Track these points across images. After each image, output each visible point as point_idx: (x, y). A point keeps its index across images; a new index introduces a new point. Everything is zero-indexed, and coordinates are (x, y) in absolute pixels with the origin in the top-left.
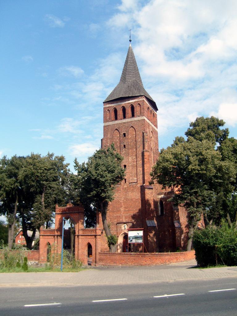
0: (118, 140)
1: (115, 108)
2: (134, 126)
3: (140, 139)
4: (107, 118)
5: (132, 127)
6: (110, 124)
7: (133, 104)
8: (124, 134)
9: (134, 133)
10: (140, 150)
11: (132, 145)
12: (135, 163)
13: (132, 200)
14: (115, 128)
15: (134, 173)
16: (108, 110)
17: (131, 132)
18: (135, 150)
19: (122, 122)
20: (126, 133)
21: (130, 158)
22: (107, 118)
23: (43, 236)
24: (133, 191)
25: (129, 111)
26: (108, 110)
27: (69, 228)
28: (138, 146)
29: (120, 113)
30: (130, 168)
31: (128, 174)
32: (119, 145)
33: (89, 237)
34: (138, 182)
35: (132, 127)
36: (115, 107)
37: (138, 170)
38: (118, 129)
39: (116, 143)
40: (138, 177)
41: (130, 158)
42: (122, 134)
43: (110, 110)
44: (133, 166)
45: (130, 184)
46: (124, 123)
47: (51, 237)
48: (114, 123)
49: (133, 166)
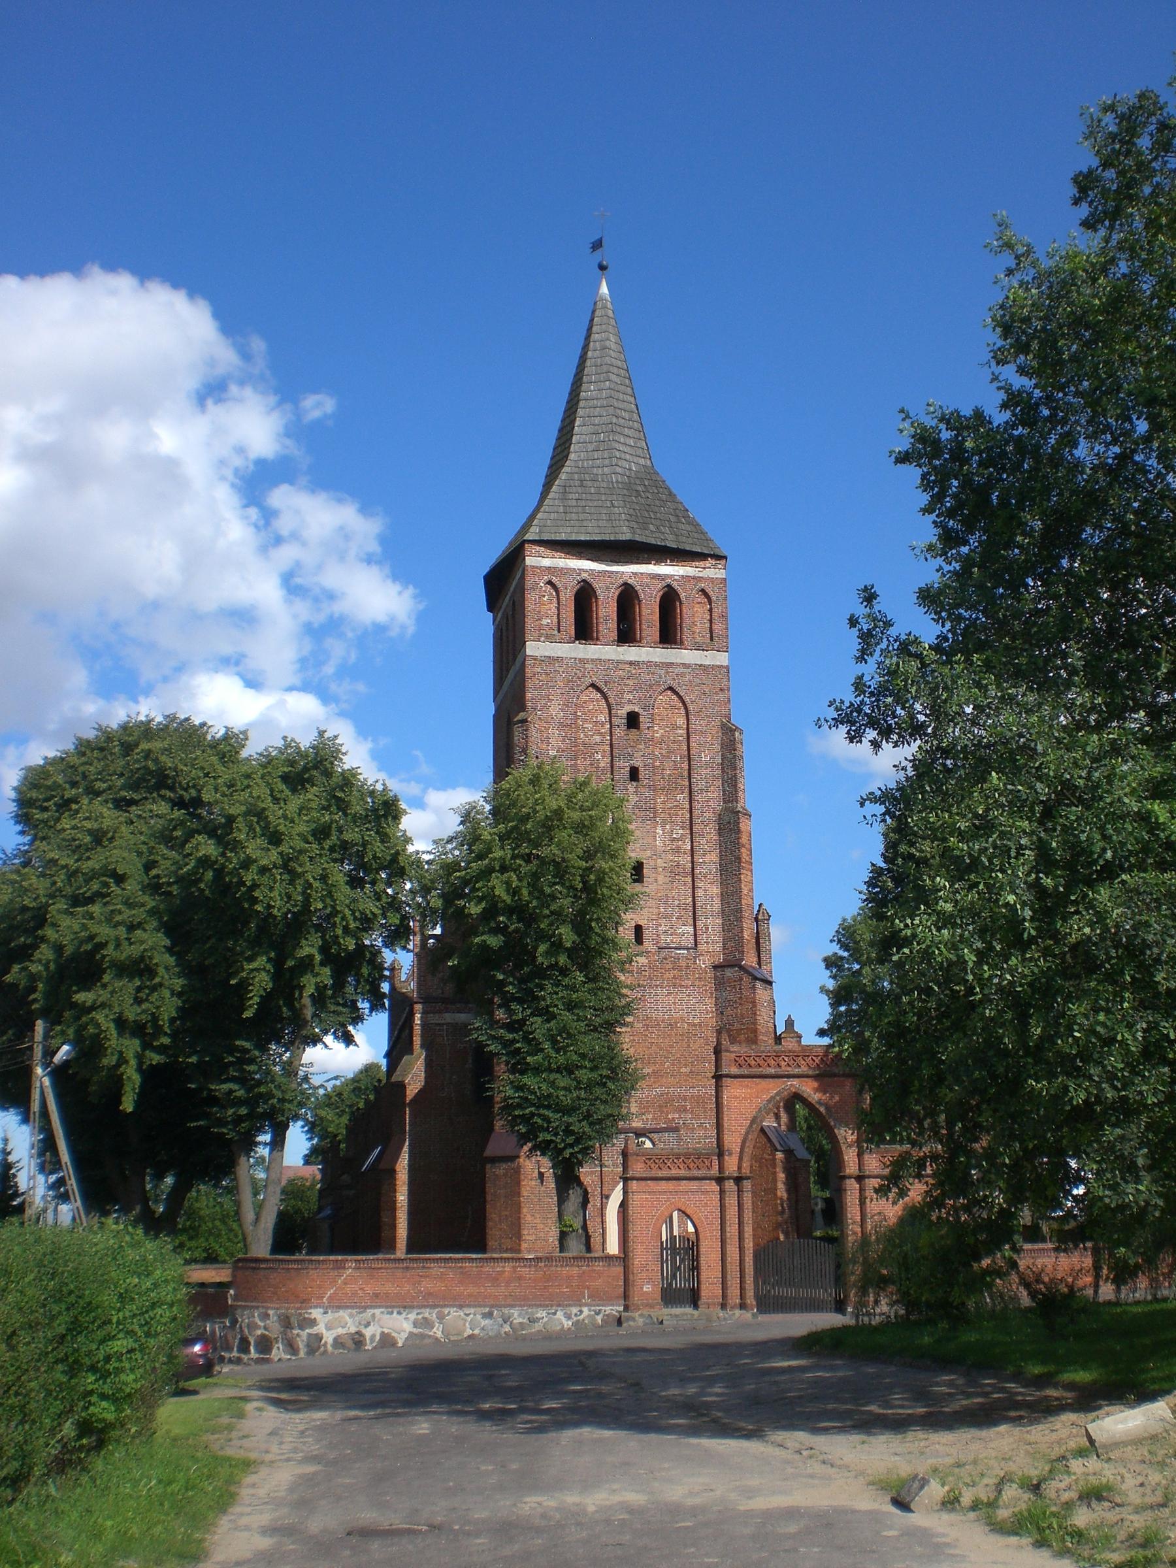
0: (597, 738)
1: (584, 581)
2: (678, 689)
3: (707, 752)
4: (544, 622)
5: (671, 689)
6: (560, 654)
7: (675, 585)
8: (633, 720)
9: (681, 721)
10: (710, 799)
11: (668, 772)
12: (685, 861)
13: (672, 1025)
14: (589, 681)
15: (677, 902)
16: (550, 583)
17: (664, 712)
18: (682, 798)
19: (622, 657)
20: (641, 712)
21: (659, 830)
22: (544, 622)
23: (643, 1183)
24: (676, 984)
25: (649, 613)
26: (550, 583)
27: (800, 1037)
28: (699, 782)
29: (606, 612)
30: (661, 878)
31: (651, 903)
32: (604, 764)
33: (663, 1185)
34: (702, 947)
35: (671, 689)
36: (585, 576)
37: (700, 893)
38: (601, 685)
39: (591, 749)
40: (700, 925)
41: (659, 830)
42: (623, 712)
43: (559, 585)
44: (674, 871)
45: (665, 952)
46: (631, 663)
47: (696, 1183)
48: (581, 656)
49: (674, 871)
